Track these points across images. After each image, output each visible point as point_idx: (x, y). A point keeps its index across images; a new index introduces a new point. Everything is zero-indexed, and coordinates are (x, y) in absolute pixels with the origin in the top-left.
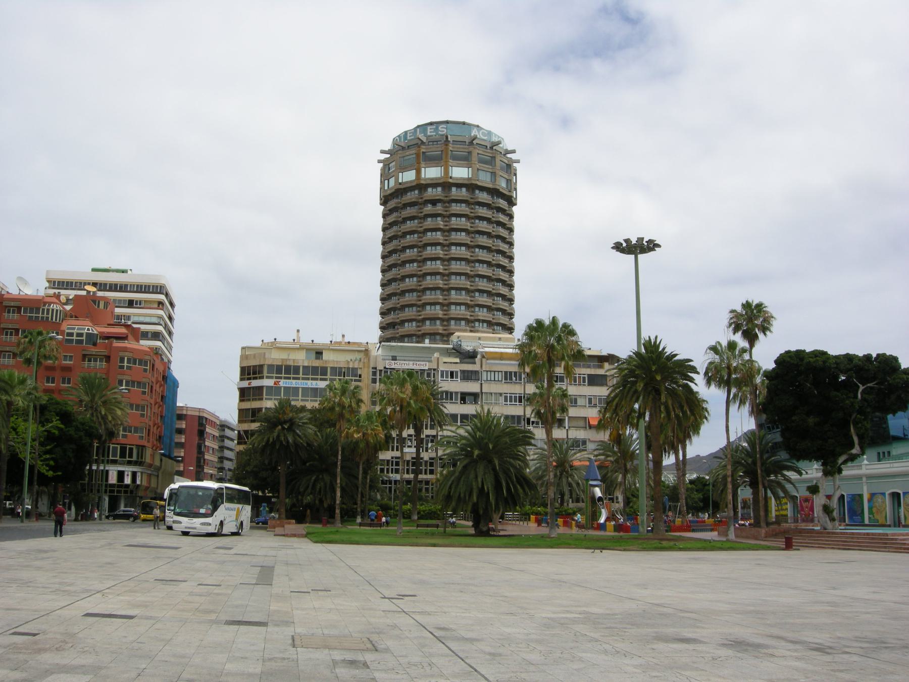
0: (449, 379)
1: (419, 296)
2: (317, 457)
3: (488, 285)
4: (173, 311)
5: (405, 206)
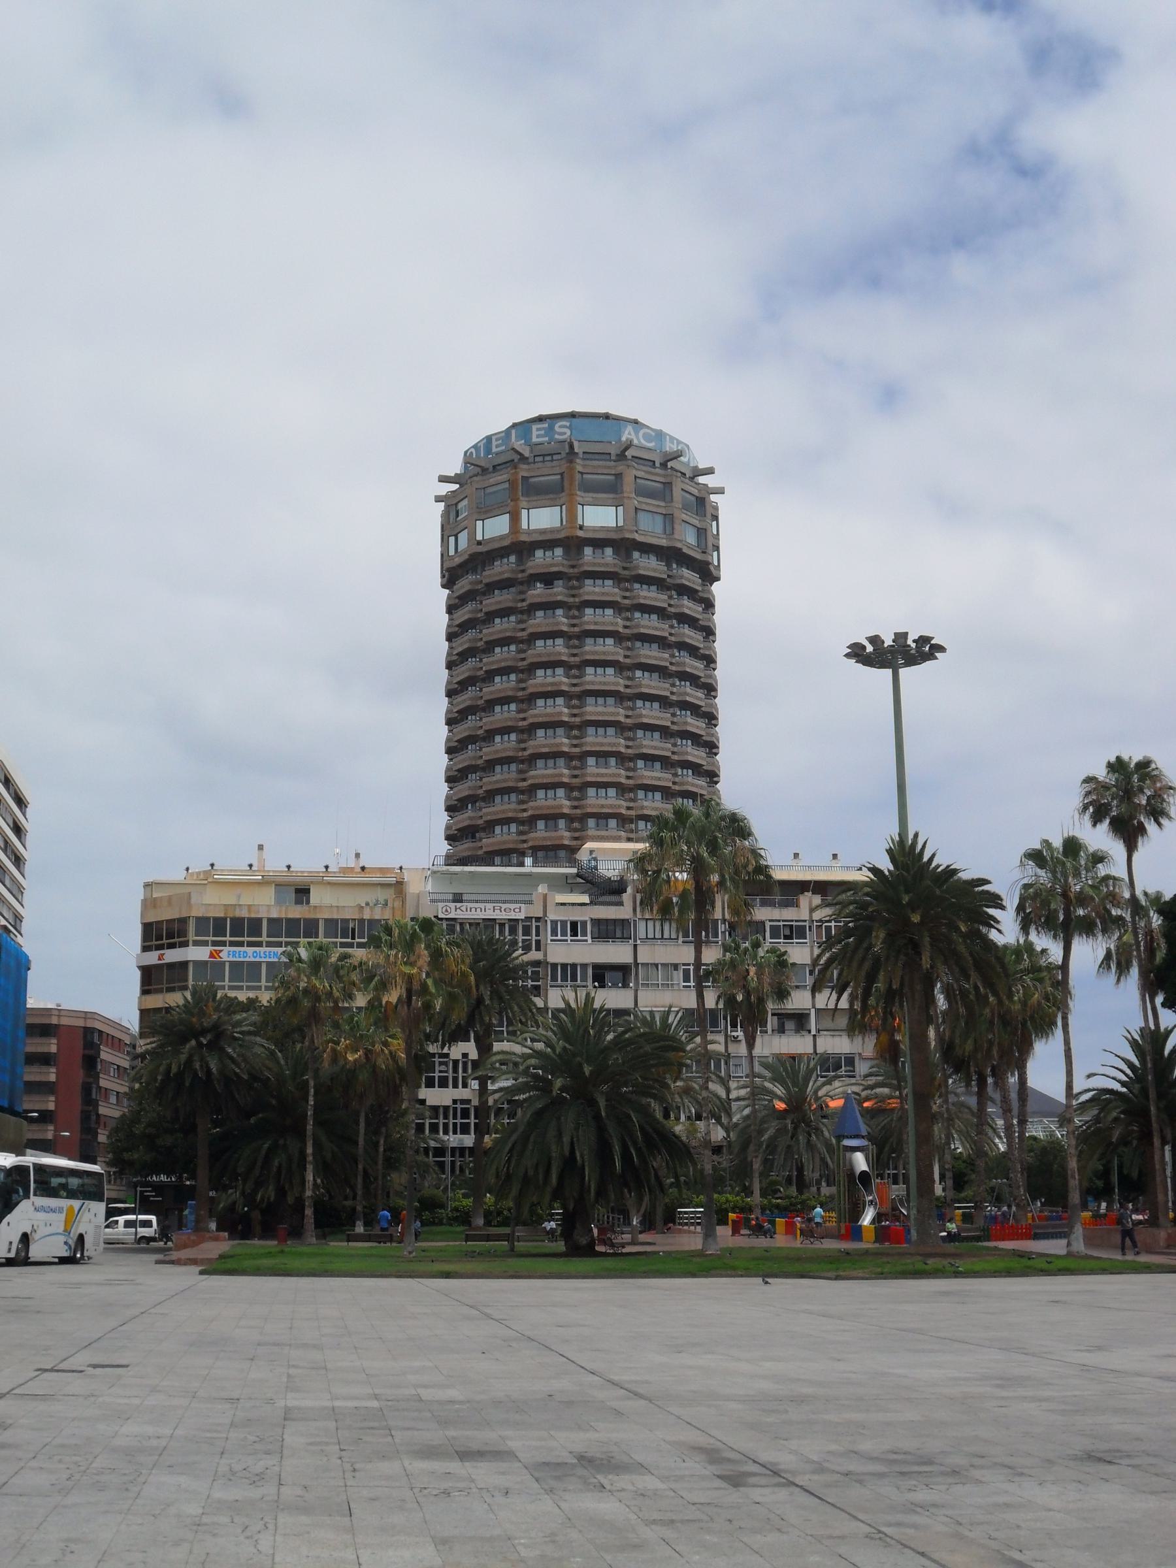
0: (569, 938)
1: (520, 772)
2: (274, 1102)
3: (662, 745)
4: (24, 814)
5: (491, 588)
